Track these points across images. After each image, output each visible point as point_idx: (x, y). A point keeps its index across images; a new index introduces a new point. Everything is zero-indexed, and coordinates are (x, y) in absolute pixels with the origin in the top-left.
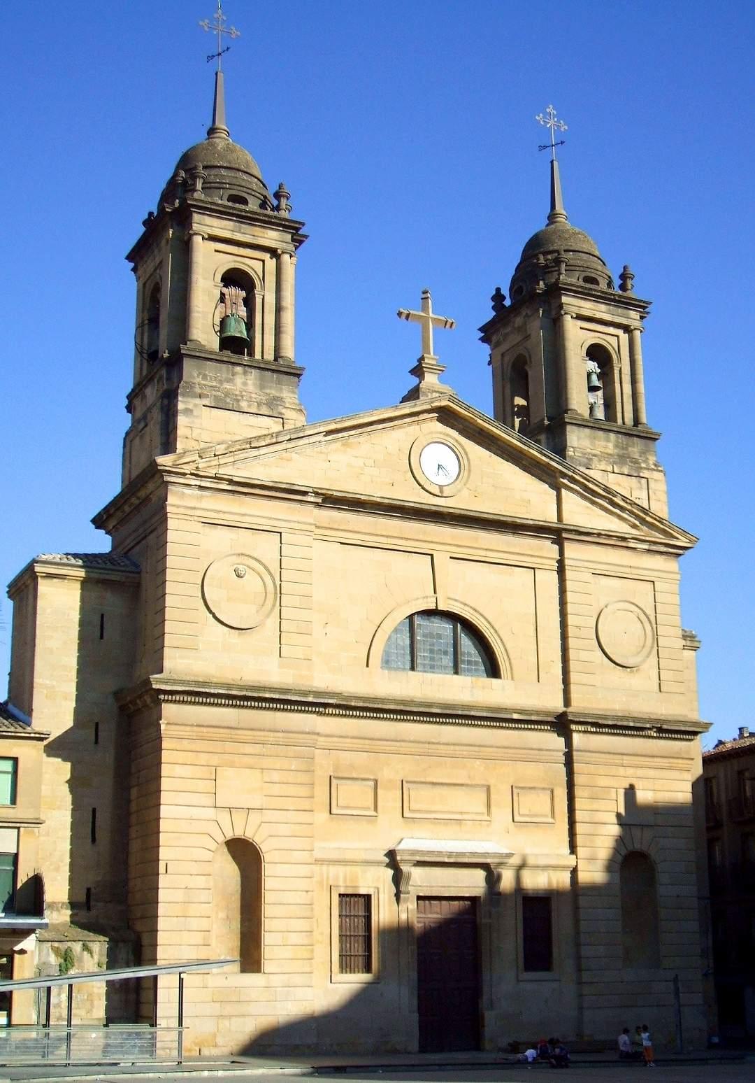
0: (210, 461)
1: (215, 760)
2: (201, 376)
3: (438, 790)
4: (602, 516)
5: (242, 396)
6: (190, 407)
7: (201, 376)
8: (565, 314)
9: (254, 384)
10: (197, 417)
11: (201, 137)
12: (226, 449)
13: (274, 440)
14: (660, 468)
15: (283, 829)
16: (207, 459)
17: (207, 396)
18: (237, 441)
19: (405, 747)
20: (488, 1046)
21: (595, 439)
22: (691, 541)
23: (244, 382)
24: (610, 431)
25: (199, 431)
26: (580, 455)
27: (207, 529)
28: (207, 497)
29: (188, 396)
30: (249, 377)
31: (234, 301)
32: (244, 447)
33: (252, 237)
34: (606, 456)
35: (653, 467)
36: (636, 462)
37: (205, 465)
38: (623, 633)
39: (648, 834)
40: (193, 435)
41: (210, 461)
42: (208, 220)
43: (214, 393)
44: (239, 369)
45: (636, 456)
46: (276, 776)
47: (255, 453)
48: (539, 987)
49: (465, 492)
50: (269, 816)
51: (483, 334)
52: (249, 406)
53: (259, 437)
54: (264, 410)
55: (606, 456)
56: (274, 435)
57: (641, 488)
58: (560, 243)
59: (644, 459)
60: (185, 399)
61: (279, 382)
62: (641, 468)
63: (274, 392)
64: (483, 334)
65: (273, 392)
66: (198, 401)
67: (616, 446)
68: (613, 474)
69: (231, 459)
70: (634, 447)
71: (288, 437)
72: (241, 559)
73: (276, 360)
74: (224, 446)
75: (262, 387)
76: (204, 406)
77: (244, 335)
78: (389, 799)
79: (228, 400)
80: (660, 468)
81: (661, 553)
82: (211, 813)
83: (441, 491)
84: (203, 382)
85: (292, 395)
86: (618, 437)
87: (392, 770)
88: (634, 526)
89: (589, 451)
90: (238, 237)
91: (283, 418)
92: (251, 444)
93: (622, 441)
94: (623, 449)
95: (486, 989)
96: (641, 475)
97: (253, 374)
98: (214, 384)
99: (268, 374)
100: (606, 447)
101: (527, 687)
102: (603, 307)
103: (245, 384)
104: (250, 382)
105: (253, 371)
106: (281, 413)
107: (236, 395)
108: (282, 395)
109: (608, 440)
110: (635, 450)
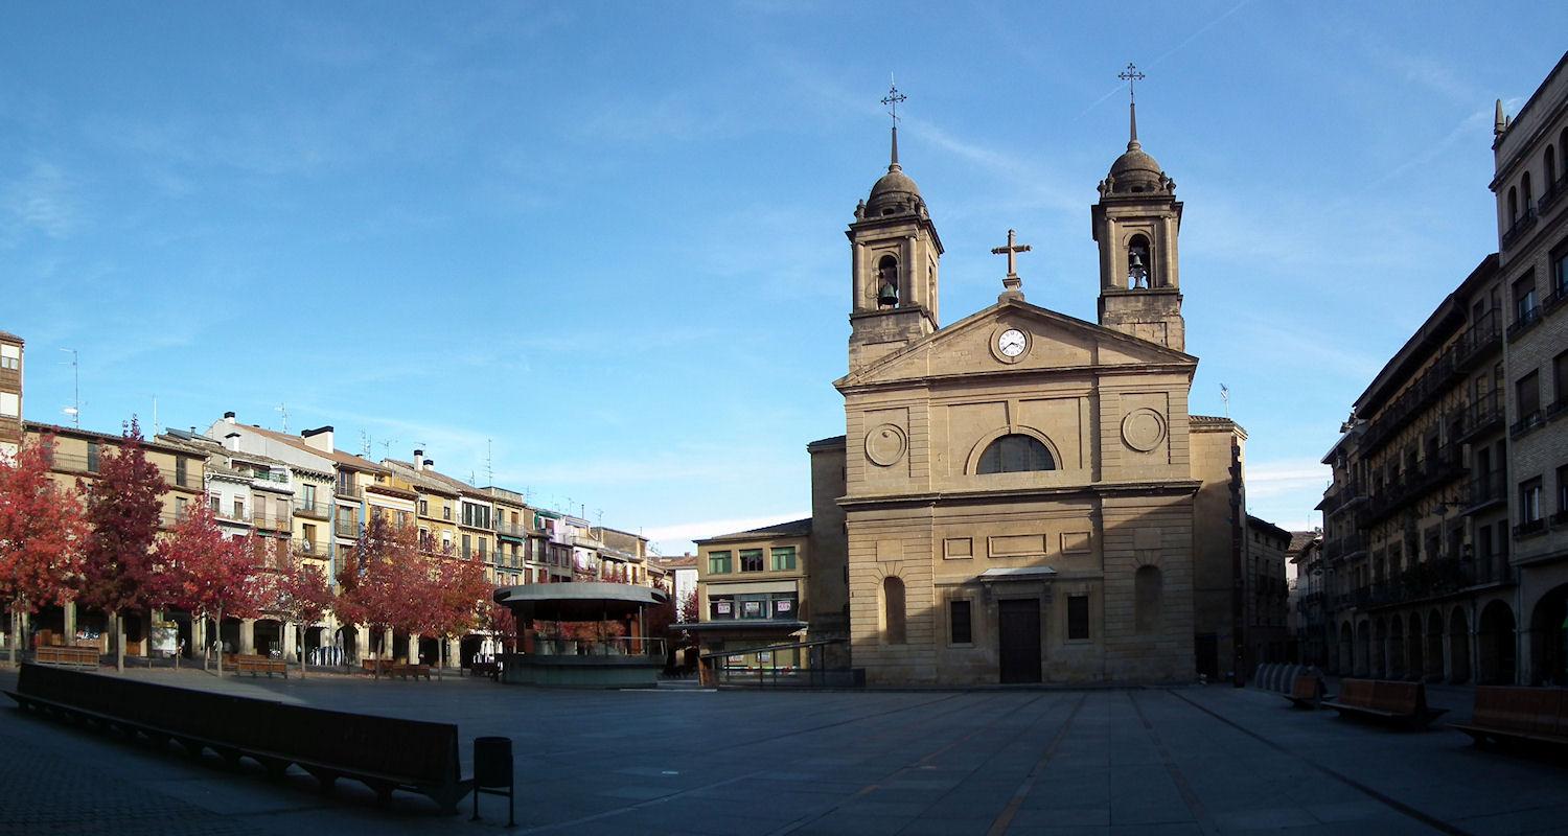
1: (876, 537)
3: (1012, 540)
15: (915, 570)
19: (989, 518)
20: (1043, 680)
27: (868, 414)
34: (1135, 313)
38: (1141, 429)
39: (1158, 554)
44: (884, 317)
46: (912, 542)
47: (890, 365)
48: (1079, 647)
50: (906, 563)
55: (1135, 313)
66: (858, 343)
67: (1144, 304)
72: (888, 427)
73: (935, 329)
77: (1290, 548)
78: (979, 548)
82: (875, 565)
87: (981, 531)
90: (882, 237)
92: (885, 360)
95: (1043, 649)
99: (901, 316)
101: (1071, 474)
102: (1140, 208)
103: (888, 325)
109: (1138, 301)
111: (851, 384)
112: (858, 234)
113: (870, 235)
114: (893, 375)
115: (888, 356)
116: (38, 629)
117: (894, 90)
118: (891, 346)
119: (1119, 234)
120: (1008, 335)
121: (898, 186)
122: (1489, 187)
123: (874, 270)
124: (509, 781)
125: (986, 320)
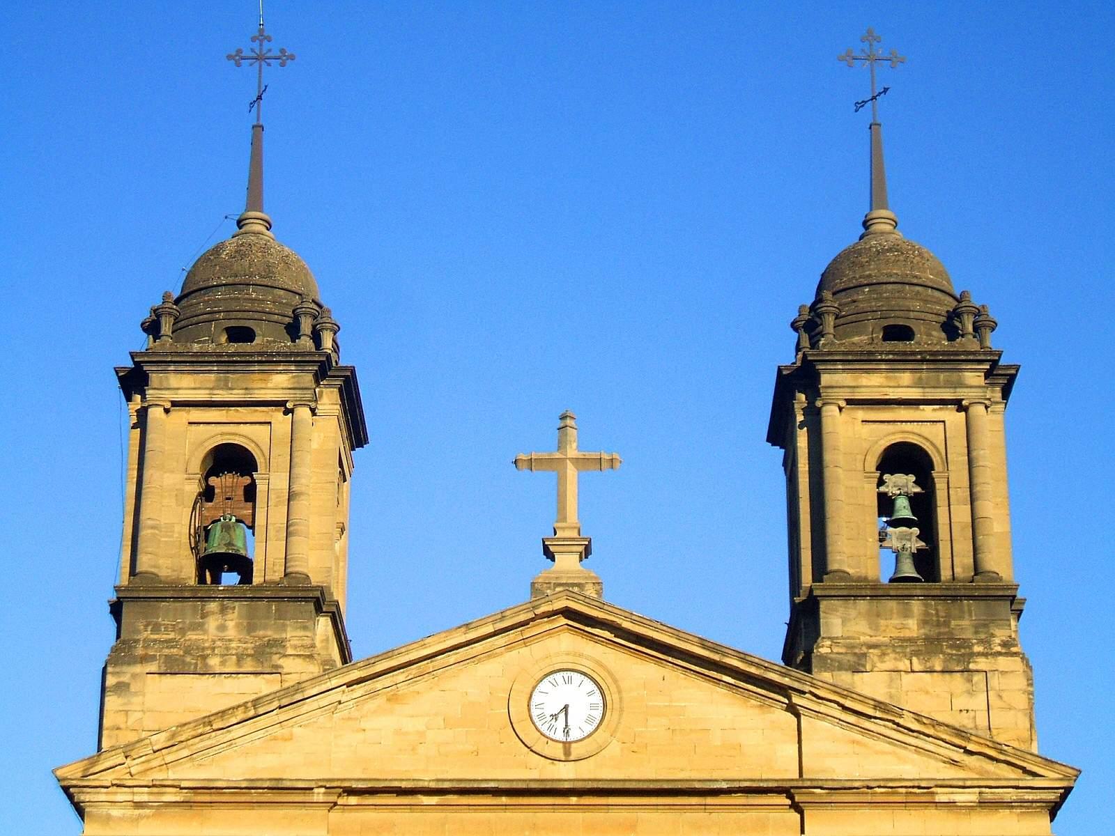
0: (148, 761)
2: (150, 628)
4: (883, 753)
5: (213, 649)
6: (125, 679)
7: (150, 628)
8: (824, 404)
9: (238, 626)
10: (136, 694)
11: (225, 233)
12: (169, 740)
13: (252, 713)
14: (1014, 649)
16: (143, 759)
17: (153, 658)
18: (185, 724)
21: (878, 615)
22: (1066, 778)
23: (222, 626)
24: (911, 597)
25: (139, 715)
26: (843, 650)
28: (148, 817)
29: (123, 664)
30: (229, 616)
31: (229, 495)
32: (200, 731)
33: (243, 391)
34: (903, 645)
35: (999, 649)
36: (965, 644)
37: (140, 768)
40: (129, 723)
41: (148, 761)
42: (174, 380)
43: (166, 651)
45: (968, 634)
49: (615, 748)
51: (806, 428)
52: (223, 663)
53: (223, 712)
54: (249, 666)
55: (903, 645)
56: (249, 705)
57: (971, 693)
58: (851, 274)
59: (983, 636)
60: (117, 669)
61: (280, 616)
62: (972, 655)
63: (271, 634)
64: (806, 428)
65: (269, 633)
66: (138, 669)
67: (924, 623)
68: (912, 675)
69: (185, 753)
70: (961, 618)
71: (276, 704)
74: (163, 736)
75: (250, 628)
76: (147, 674)
79: (188, 659)
80: (1014, 649)
81: (1009, 805)
83: (567, 752)
84: (156, 637)
85: (301, 633)
86: (926, 606)
88: (954, 763)
89: (863, 639)
91: (280, 673)
93: (937, 611)
94: (938, 625)
96: (972, 666)
97: (236, 611)
98: (172, 636)
100: (904, 627)
102: (906, 378)
103: (222, 628)
104: (231, 624)
105: (237, 604)
106: (277, 667)
107: (203, 649)
108: (284, 636)
109: (907, 614)
110: (965, 623)
111: (107, 778)
112: (154, 379)
113: (185, 385)
114: (236, 762)
115: (222, 714)
116: (327, 374)
117: (261, 37)
118: (230, 684)
119: (853, 438)
120: (593, 707)
121: (269, 271)
122: (768, 441)
123: (1010, 549)
124: (120, 379)
125: (500, 640)
